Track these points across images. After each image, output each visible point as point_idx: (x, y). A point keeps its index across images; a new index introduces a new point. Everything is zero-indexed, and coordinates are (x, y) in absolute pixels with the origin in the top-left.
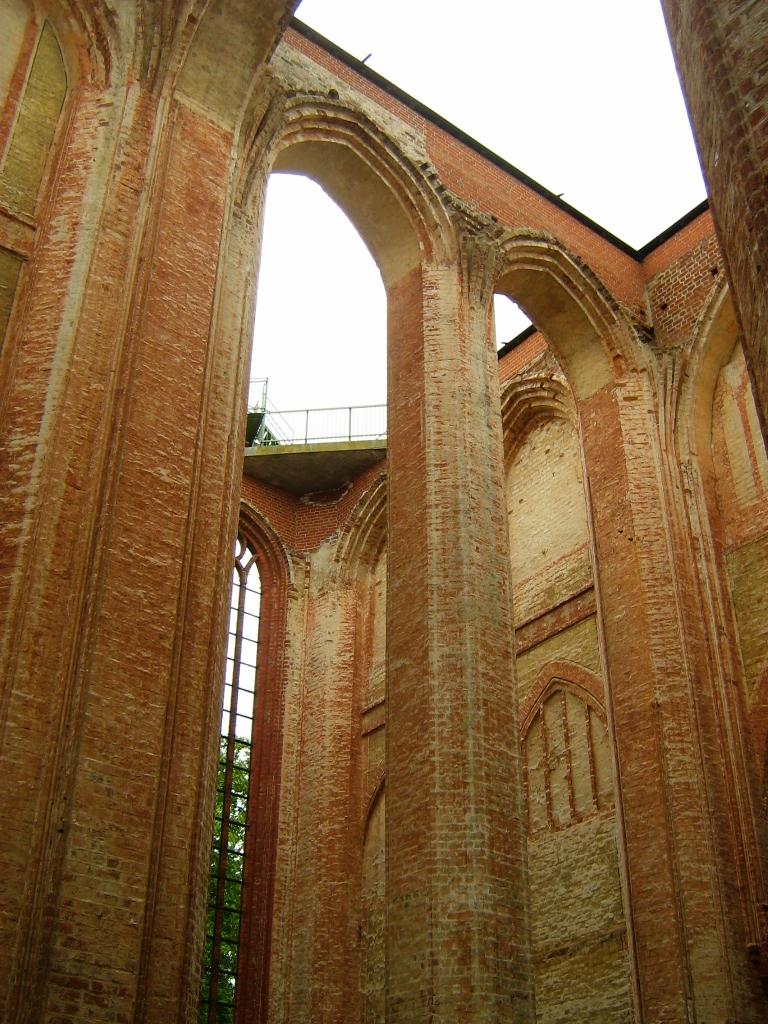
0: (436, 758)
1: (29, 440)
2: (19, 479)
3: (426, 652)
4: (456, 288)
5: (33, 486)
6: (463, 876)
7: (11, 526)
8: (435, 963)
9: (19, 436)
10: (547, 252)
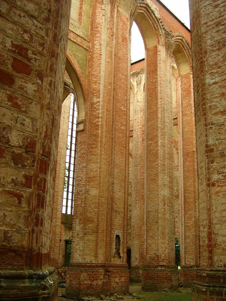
0: (159, 164)
1: (98, 100)
2: (97, 109)
3: (157, 142)
4: (165, 53)
5: (100, 111)
6: (164, 188)
7: (97, 120)
8: (159, 205)
9: (95, 99)
10: (180, 39)
